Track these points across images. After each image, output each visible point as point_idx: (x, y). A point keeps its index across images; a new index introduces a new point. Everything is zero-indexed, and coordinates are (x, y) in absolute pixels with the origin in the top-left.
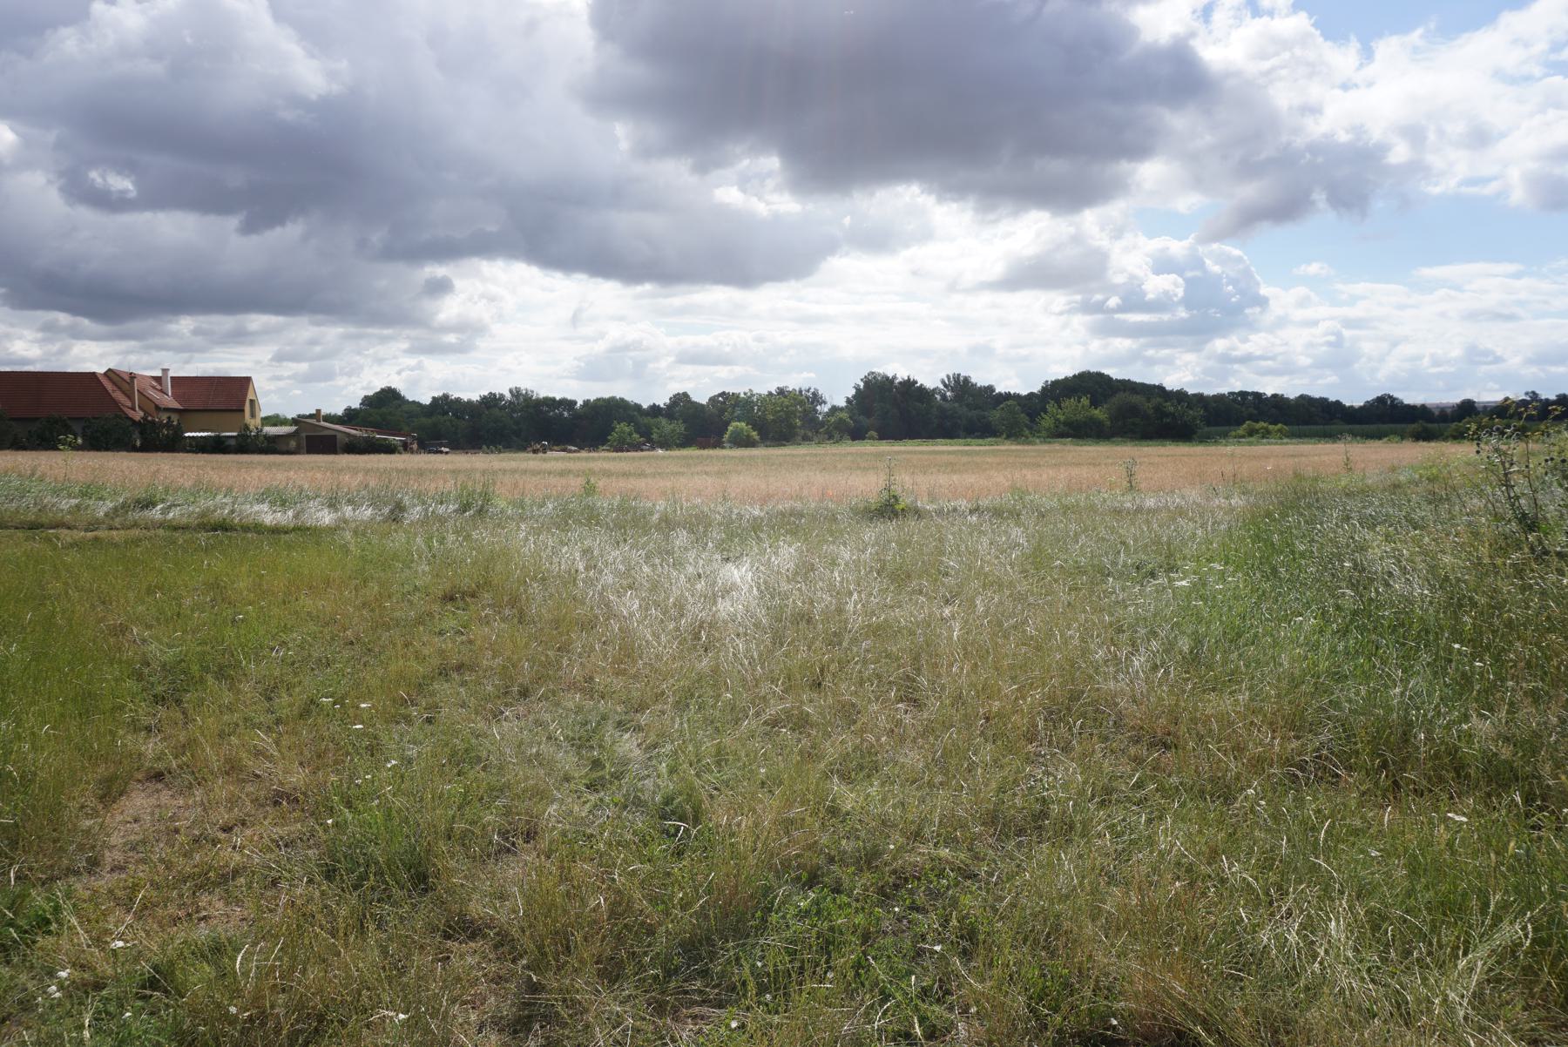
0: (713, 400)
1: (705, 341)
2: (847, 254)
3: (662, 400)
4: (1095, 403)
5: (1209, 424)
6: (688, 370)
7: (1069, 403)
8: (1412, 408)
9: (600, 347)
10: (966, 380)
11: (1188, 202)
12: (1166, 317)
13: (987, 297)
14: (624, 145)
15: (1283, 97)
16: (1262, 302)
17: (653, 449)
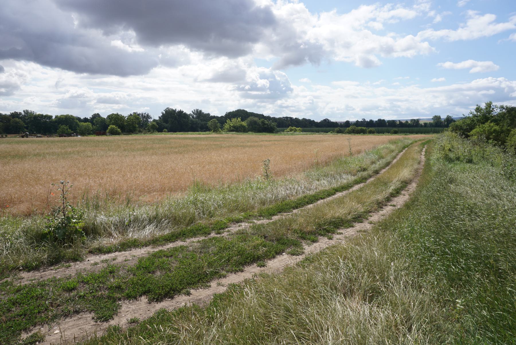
0: (109, 116)
1: (108, 95)
2: (161, 67)
3: (89, 116)
4: (242, 120)
5: (279, 127)
6: (102, 105)
7: (234, 120)
8: (333, 123)
9: (67, 96)
10: (200, 111)
11: (270, 57)
12: (264, 93)
13: (207, 84)
14: (76, 23)
15: (297, 27)
16: (291, 90)
17: (77, 135)
